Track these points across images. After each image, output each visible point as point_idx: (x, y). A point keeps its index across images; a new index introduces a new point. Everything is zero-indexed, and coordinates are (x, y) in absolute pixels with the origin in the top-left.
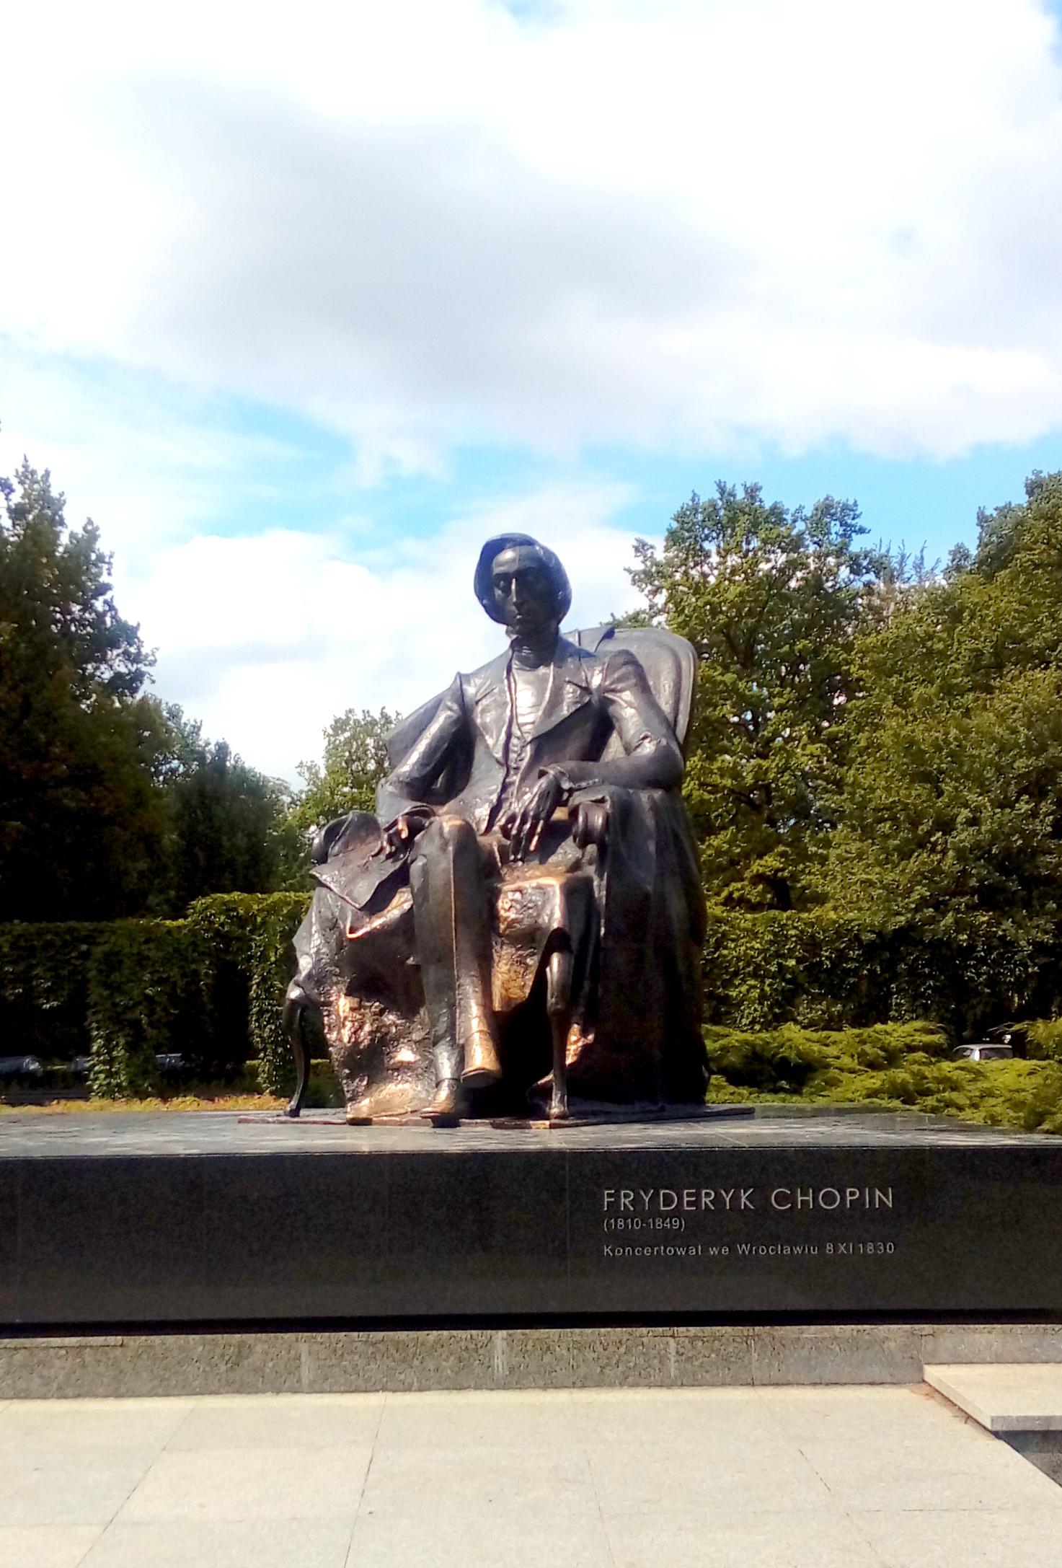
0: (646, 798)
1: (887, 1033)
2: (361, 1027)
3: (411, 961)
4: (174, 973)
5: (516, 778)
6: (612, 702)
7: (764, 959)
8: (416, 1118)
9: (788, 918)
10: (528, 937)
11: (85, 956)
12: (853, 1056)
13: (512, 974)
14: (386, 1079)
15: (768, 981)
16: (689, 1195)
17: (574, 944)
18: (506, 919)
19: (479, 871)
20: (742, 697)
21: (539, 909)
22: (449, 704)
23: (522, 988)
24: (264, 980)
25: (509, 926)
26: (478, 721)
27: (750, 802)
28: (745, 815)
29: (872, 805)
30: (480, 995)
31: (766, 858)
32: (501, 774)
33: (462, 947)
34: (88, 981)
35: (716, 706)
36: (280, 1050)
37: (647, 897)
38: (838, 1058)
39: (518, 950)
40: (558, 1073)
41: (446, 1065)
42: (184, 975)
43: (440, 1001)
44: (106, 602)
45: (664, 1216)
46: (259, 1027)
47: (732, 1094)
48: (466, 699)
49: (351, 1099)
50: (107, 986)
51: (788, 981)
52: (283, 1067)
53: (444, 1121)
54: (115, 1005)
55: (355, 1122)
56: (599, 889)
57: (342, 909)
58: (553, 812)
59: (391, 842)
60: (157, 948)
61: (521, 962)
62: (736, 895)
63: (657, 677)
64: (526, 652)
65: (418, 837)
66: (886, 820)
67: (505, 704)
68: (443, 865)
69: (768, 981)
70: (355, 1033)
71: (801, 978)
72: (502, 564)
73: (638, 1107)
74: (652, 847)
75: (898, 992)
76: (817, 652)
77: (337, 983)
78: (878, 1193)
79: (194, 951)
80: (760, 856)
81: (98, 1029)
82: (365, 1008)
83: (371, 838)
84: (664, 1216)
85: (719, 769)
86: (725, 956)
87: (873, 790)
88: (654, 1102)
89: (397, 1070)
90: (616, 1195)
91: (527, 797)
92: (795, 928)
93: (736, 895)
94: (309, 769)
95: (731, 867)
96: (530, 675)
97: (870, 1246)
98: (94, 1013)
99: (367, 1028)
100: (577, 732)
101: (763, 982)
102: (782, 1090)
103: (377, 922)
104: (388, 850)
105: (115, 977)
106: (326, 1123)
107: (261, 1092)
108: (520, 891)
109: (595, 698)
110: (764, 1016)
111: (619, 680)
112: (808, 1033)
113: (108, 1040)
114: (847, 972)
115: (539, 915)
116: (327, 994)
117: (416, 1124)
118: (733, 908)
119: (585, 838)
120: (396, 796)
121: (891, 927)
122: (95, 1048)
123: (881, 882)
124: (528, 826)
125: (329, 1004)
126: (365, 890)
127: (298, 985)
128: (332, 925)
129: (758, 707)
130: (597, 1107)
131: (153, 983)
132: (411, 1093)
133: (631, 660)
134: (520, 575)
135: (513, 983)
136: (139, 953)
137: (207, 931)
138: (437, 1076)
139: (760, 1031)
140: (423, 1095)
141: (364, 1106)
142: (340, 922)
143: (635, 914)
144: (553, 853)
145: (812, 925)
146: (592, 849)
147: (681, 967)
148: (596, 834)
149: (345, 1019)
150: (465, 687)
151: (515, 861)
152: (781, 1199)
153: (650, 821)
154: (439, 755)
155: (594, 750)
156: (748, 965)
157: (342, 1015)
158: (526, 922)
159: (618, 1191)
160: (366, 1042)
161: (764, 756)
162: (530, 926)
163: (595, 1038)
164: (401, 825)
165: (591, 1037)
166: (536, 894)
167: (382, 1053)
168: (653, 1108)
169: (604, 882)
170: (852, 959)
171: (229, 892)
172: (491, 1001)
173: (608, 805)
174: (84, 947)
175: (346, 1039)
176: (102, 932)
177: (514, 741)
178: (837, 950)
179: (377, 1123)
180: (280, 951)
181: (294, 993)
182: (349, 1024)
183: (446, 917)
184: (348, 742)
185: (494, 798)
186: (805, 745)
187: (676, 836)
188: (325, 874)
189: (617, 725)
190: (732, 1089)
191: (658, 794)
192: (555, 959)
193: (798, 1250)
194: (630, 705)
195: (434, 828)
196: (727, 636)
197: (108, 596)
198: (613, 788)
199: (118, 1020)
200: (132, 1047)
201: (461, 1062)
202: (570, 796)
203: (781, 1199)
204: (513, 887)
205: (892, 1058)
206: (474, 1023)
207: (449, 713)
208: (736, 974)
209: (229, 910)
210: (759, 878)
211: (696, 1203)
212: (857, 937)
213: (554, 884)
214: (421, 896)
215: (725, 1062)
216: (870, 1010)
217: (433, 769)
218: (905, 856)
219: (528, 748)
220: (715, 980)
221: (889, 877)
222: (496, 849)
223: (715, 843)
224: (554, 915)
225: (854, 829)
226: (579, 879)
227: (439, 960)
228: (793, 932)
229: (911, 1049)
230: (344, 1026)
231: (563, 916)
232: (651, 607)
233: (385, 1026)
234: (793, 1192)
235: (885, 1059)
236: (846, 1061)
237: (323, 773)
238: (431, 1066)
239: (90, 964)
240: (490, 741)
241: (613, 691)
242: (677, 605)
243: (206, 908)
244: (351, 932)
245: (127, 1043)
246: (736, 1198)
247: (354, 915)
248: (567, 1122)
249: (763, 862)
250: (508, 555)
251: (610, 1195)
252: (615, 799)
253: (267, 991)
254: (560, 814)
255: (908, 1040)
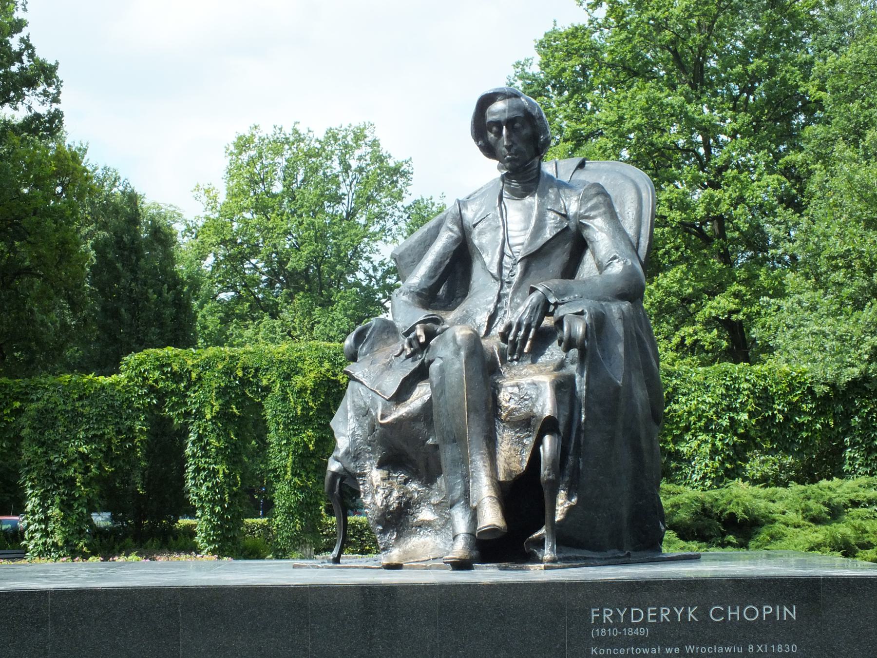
0: (616, 309)
1: (830, 489)
2: (390, 494)
3: (430, 441)
4: (110, 430)
5: (509, 291)
6: (586, 226)
7: (716, 413)
8: (439, 563)
9: (740, 371)
10: (525, 423)
11: (19, 412)
12: (797, 511)
13: (512, 452)
14: (410, 534)
15: (719, 436)
16: (652, 611)
17: (561, 428)
18: (507, 408)
19: (485, 369)
20: (690, 120)
21: (534, 401)
22: (450, 226)
23: (521, 464)
24: (200, 438)
25: (510, 414)
26: (476, 242)
27: (701, 233)
28: (696, 249)
29: (826, 253)
30: (488, 468)
31: (718, 298)
32: (496, 287)
33: (474, 432)
34: (22, 439)
35: (663, 131)
36: (218, 509)
37: (617, 389)
38: (784, 513)
39: (516, 433)
40: (549, 527)
41: (461, 521)
42: (119, 432)
43: (456, 473)
44: (22, 40)
45: (634, 626)
46: (195, 485)
47: (682, 549)
48: (465, 222)
49: (384, 550)
50: (42, 444)
51: (741, 436)
52: (221, 527)
53: (460, 565)
54: (49, 462)
55: (390, 567)
56: (581, 385)
57: (373, 399)
58: (543, 320)
59: (410, 345)
60: (91, 405)
61: (520, 441)
62: (688, 341)
63: (623, 204)
64: (514, 184)
65: (432, 342)
66: (841, 267)
67: (499, 227)
68: (457, 366)
69: (719, 436)
70: (386, 498)
71: (752, 433)
72: (494, 114)
73: (609, 553)
74: (621, 349)
75: (852, 446)
76: (772, 72)
77: (370, 458)
78: (785, 609)
79: (129, 407)
80: (712, 294)
81: (32, 487)
82: (393, 478)
83: (391, 341)
84: (634, 626)
85: (667, 200)
86: (675, 411)
87: (827, 237)
88: (621, 549)
89: (420, 526)
90: (601, 612)
91: (521, 309)
92: (747, 381)
93: (688, 341)
94: (207, 191)
95: (681, 309)
96: (518, 204)
97: (780, 647)
98: (28, 472)
99: (395, 494)
100: (559, 251)
101: (714, 437)
102: (730, 543)
103: (402, 411)
104: (409, 352)
105: (49, 434)
106: (366, 568)
107: (192, 549)
108: (518, 385)
109: (572, 225)
110: (716, 471)
111: (593, 208)
112: (758, 490)
113: (43, 498)
114: (800, 426)
115: (534, 405)
116: (362, 467)
117: (439, 567)
118: (686, 353)
119: (569, 344)
120: (410, 305)
121: (845, 379)
122: (29, 507)
123: (834, 333)
124: (521, 333)
125: (363, 475)
126: (391, 384)
127: (337, 459)
128: (364, 413)
129: (709, 131)
130: (577, 553)
131: (88, 441)
132: (431, 545)
133: (601, 191)
134: (510, 123)
135: (513, 459)
136: (73, 410)
137: (142, 387)
138: (453, 530)
139: (711, 488)
140: (442, 546)
141: (394, 555)
142: (371, 410)
143: (608, 401)
144: (542, 354)
145: (765, 377)
146: (574, 352)
147: (644, 445)
148: (578, 340)
149: (378, 488)
150: (463, 212)
151: (512, 361)
152: (717, 614)
153: (619, 329)
154: (442, 269)
155: (570, 270)
156: (700, 420)
157: (375, 484)
158: (524, 411)
159: (602, 610)
160: (395, 505)
161: (715, 186)
162: (527, 414)
163: (578, 501)
164: (419, 332)
165: (574, 500)
166: (530, 387)
167: (407, 513)
168: (621, 555)
169: (584, 379)
170: (805, 413)
171: (162, 347)
172: (497, 473)
173: (586, 317)
174: (17, 404)
175: (379, 504)
176: (35, 388)
177: (506, 259)
178: (790, 403)
179: (406, 568)
180: (217, 408)
181: (334, 466)
182: (381, 491)
183: (460, 407)
184: (252, 162)
185: (491, 307)
186: (761, 174)
187: (639, 337)
188: (357, 369)
189: (590, 246)
190: (682, 543)
191: (625, 305)
192: (547, 439)
193: (728, 650)
194: (601, 230)
195: (448, 334)
196: (674, 52)
197: (23, 34)
198: (589, 302)
199: (53, 480)
200: (66, 506)
201: (474, 518)
202: (556, 308)
203: (717, 614)
204: (512, 382)
205: (835, 513)
206: (484, 492)
207: (451, 233)
208: (687, 429)
209: (162, 366)
210: (710, 323)
211: (657, 617)
212: (810, 391)
213: (546, 381)
214: (439, 390)
215: (676, 519)
216: (823, 463)
217: (437, 281)
218: (859, 306)
219: (519, 266)
220: (665, 435)
221: (842, 329)
222: (496, 351)
223: (665, 282)
224: (546, 406)
225: (807, 277)
226: (564, 377)
227: (454, 441)
228: (745, 385)
229: (855, 504)
230: (377, 492)
231: (554, 407)
232: (591, 22)
233: (408, 492)
234: (726, 609)
235: (828, 514)
236: (792, 516)
237: (222, 198)
238: (448, 522)
239: (24, 420)
240: (487, 259)
241: (587, 218)
242: (619, 18)
243: (140, 364)
244: (382, 419)
245: (62, 501)
246: (685, 613)
247: (384, 405)
248: (557, 565)
249: (715, 304)
250: (499, 106)
251: (595, 612)
252: (593, 311)
253: (203, 448)
254: (548, 322)
255: (852, 496)
